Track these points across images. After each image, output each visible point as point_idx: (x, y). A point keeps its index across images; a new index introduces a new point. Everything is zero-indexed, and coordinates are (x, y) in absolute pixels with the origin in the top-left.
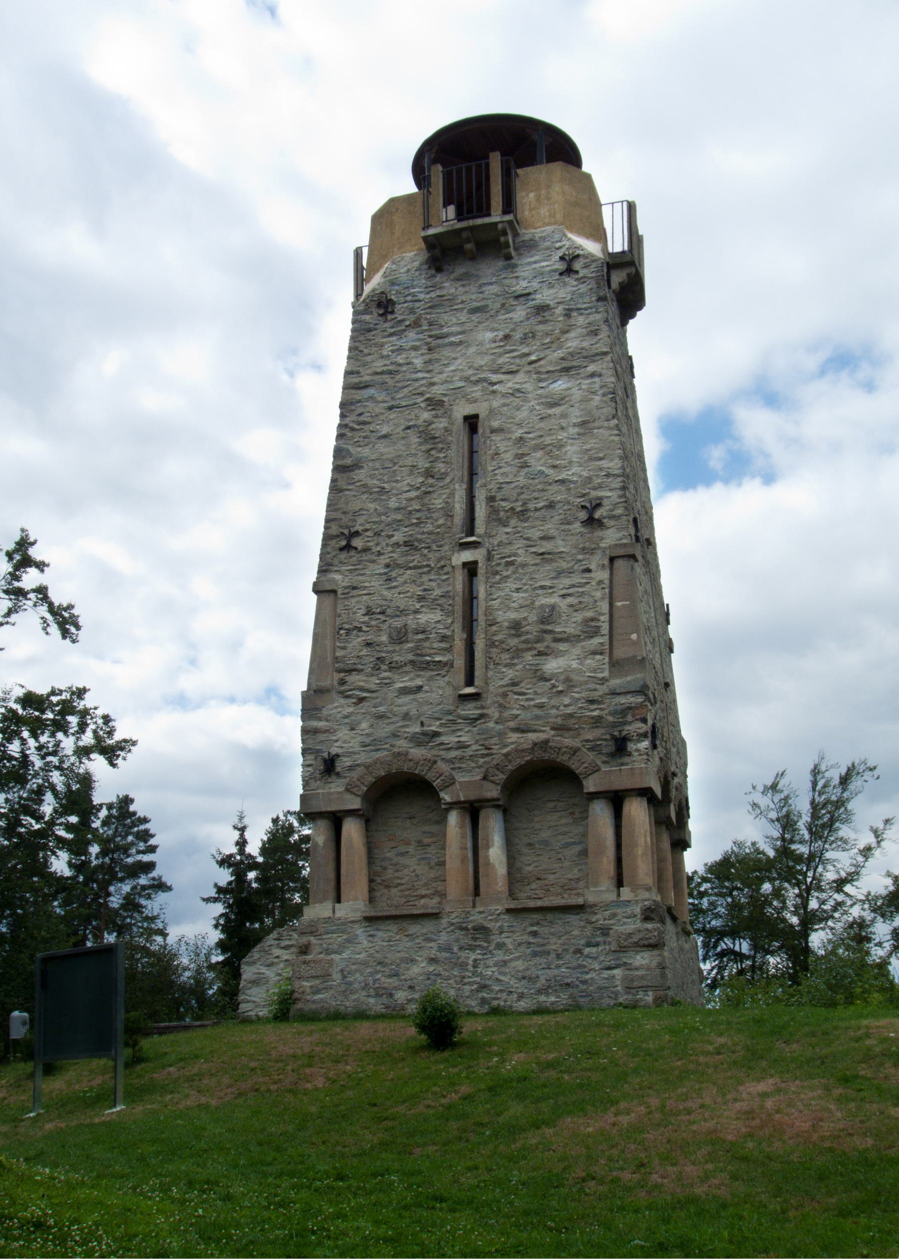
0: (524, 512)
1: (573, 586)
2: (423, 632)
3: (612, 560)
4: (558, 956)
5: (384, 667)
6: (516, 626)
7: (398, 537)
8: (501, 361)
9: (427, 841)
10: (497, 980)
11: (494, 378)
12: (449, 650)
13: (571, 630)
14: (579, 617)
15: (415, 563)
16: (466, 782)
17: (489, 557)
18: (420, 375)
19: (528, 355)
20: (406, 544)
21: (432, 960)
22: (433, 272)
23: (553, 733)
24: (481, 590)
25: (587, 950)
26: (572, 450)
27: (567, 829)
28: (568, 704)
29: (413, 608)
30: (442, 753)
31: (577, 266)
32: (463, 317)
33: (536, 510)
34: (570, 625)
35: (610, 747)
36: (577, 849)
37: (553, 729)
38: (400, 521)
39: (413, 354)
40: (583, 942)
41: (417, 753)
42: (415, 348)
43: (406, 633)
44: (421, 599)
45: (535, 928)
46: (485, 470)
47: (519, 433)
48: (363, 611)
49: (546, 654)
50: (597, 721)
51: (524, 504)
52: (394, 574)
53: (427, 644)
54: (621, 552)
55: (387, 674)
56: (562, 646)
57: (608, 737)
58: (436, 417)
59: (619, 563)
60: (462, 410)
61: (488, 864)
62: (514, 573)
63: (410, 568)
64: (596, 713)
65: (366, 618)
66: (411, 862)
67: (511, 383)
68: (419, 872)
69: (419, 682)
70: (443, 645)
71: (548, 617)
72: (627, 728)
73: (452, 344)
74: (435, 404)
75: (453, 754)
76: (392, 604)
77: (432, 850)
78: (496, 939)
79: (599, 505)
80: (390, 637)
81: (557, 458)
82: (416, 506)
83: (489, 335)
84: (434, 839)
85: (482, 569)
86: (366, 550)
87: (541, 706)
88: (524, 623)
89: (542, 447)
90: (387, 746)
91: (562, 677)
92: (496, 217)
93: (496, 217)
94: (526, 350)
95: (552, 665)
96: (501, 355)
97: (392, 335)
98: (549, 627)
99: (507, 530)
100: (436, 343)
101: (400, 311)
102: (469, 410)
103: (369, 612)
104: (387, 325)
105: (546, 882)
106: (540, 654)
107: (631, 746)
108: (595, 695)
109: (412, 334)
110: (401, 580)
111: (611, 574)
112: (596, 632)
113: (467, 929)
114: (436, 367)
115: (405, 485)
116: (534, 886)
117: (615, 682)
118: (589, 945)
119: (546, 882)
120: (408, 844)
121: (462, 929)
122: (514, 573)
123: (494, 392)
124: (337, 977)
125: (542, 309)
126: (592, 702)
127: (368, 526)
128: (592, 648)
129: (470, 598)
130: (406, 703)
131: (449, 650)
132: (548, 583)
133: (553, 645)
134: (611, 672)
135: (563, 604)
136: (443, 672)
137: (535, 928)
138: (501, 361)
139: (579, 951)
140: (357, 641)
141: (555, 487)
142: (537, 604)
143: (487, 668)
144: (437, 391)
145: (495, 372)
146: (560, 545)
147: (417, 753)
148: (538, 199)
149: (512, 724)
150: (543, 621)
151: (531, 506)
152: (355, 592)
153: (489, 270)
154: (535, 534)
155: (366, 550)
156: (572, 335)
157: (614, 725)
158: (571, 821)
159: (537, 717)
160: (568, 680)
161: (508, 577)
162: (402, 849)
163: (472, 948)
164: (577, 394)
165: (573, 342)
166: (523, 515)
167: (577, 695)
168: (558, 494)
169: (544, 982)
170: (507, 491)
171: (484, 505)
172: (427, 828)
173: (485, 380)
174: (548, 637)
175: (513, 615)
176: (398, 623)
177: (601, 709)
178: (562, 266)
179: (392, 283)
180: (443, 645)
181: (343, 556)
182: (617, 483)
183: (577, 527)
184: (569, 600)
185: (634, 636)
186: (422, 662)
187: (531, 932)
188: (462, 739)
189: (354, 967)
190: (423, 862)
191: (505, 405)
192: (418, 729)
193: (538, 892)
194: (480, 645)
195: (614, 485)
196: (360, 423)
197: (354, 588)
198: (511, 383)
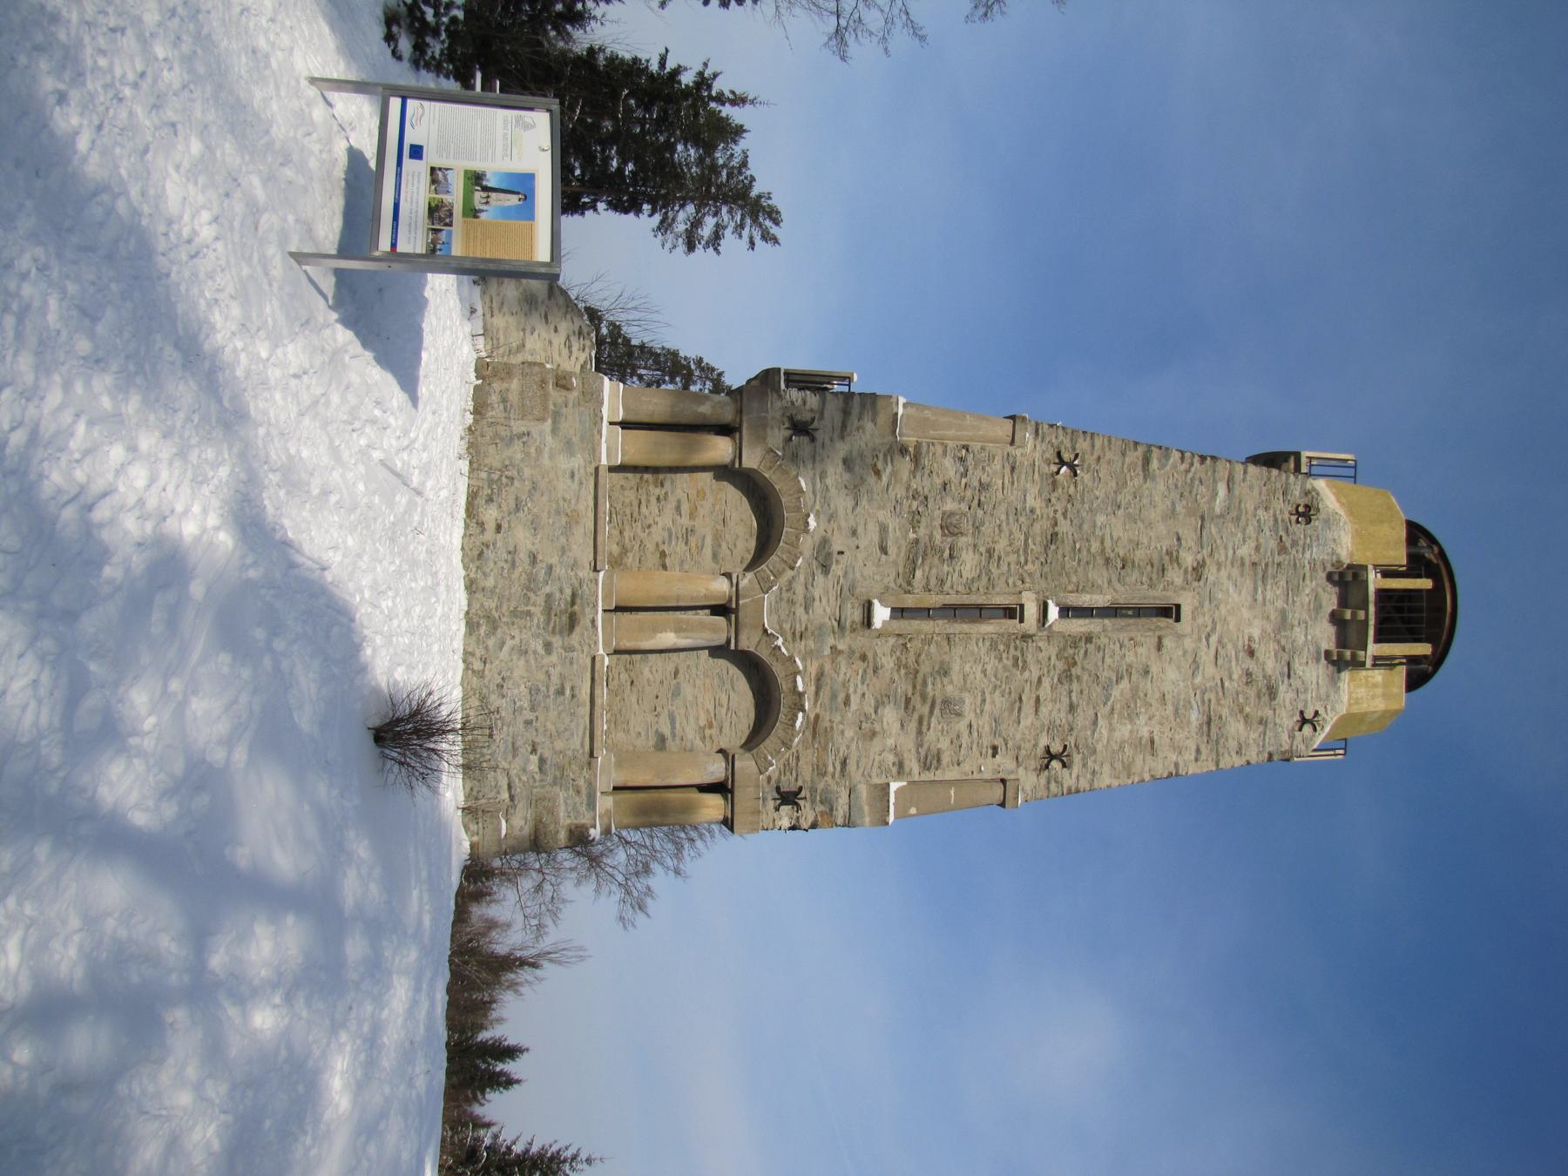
0: (1070, 677)
1: (980, 736)
2: (951, 556)
3: (1003, 781)
4: (528, 723)
5: (915, 504)
6: (944, 671)
7: (1064, 527)
8: (1229, 646)
9: (693, 541)
10: (503, 644)
11: (1214, 639)
12: (927, 589)
13: (930, 736)
14: (944, 744)
15: (1031, 546)
16: (766, 610)
17: (1026, 637)
18: (1230, 552)
19: (1230, 678)
20: (1054, 536)
21: (534, 559)
22: (1329, 568)
23: (812, 716)
24: (989, 628)
25: (534, 759)
26: (1124, 731)
27: (692, 720)
28: (846, 736)
29: (980, 542)
30: (802, 578)
31: (1307, 728)
32: (1280, 604)
33: (1071, 692)
34: (936, 736)
35: (788, 785)
36: (666, 731)
37: (817, 717)
38: (1080, 527)
39: (1253, 545)
40: (547, 754)
41: (807, 544)
42: (1257, 548)
43: (952, 534)
44: (990, 552)
45: (568, 692)
46: (1122, 629)
47: (1154, 669)
48: (985, 479)
49: (906, 708)
50: (821, 771)
51: (1078, 678)
52: (1022, 519)
53: (936, 561)
54: (1010, 794)
55: (906, 508)
56: (913, 726)
57: (800, 783)
58: (1186, 572)
59: (999, 789)
60: (1187, 602)
61: (656, 629)
62: (1005, 667)
63: (1026, 540)
64: (831, 769)
65: (976, 484)
66: (666, 519)
67: (1206, 657)
68: (653, 529)
69: (892, 550)
70: (933, 582)
71: (949, 707)
72: (808, 805)
73: (1255, 590)
74: (1198, 571)
75: (799, 588)
76: (988, 518)
77: (681, 547)
78: (557, 641)
79: (1064, 765)
80: (952, 514)
81: (1120, 714)
82: (1095, 546)
83: (1256, 633)
84: (694, 551)
85: (1011, 625)
86: (1054, 485)
87: (847, 702)
88: (946, 680)
89: (1135, 696)
90: (818, 507)
91: (877, 727)
92: (1373, 649)
93: (1373, 649)
94: (1235, 676)
95: (890, 715)
96: (1235, 646)
97: (1276, 520)
98: (937, 711)
99: (1053, 658)
100: (1259, 571)
101: (1299, 529)
102: (1186, 611)
103: (984, 487)
104: (1286, 515)
105: (628, 691)
106: (908, 701)
107: (785, 809)
108: (851, 766)
109: (1273, 544)
110: (1015, 528)
111: (987, 781)
112: (926, 766)
113: (573, 603)
114: (1235, 572)
115: (1116, 530)
116: (624, 677)
117: (863, 790)
118: (542, 761)
119: (628, 691)
120: (692, 516)
121: (574, 596)
122: (1005, 667)
123: (1200, 639)
124: (518, 426)
125: (1272, 692)
126: (844, 763)
127: (1080, 487)
128: (907, 763)
129: (979, 612)
130: (870, 537)
131: (927, 589)
132: (987, 707)
133: (916, 716)
134: (876, 786)
135: (962, 726)
136: (900, 581)
137: (568, 692)
138: (1229, 646)
139: (534, 751)
140: (950, 468)
141: (1091, 712)
142: (966, 695)
143: (899, 635)
144: (1211, 573)
145: (1220, 642)
146: (1028, 719)
147: (807, 544)
148: (1375, 686)
149: (827, 667)
150: (946, 702)
151: (1075, 686)
152: (1008, 470)
153: (1325, 636)
154: (1045, 691)
155: (1054, 485)
156: (1241, 726)
157: (813, 790)
158: (702, 723)
159: (834, 696)
160: (874, 734)
161: (1000, 659)
162: (685, 508)
163: (548, 609)
164: (1180, 736)
165: (1236, 728)
166: (1067, 676)
167: (854, 746)
168: (1082, 719)
169: (497, 704)
170: (1095, 657)
171: (1083, 629)
172: (709, 541)
173: (1214, 629)
174: (926, 710)
175: (956, 667)
176: (966, 526)
177: (833, 776)
178: (1309, 715)
179: (1327, 521)
180: (933, 582)
181: (1050, 454)
182: (1084, 784)
183: (1044, 741)
184: (965, 733)
185: (913, 811)
186: (916, 554)
187: (563, 688)
188: (817, 603)
189: (533, 450)
190: (666, 535)
191: (1185, 652)
192: (836, 547)
193: (616, 682)
194: (926, 626)
195: (1082, 780)
196: (1192, 480)
197: (1013, 469)
198: (1206, 657)
